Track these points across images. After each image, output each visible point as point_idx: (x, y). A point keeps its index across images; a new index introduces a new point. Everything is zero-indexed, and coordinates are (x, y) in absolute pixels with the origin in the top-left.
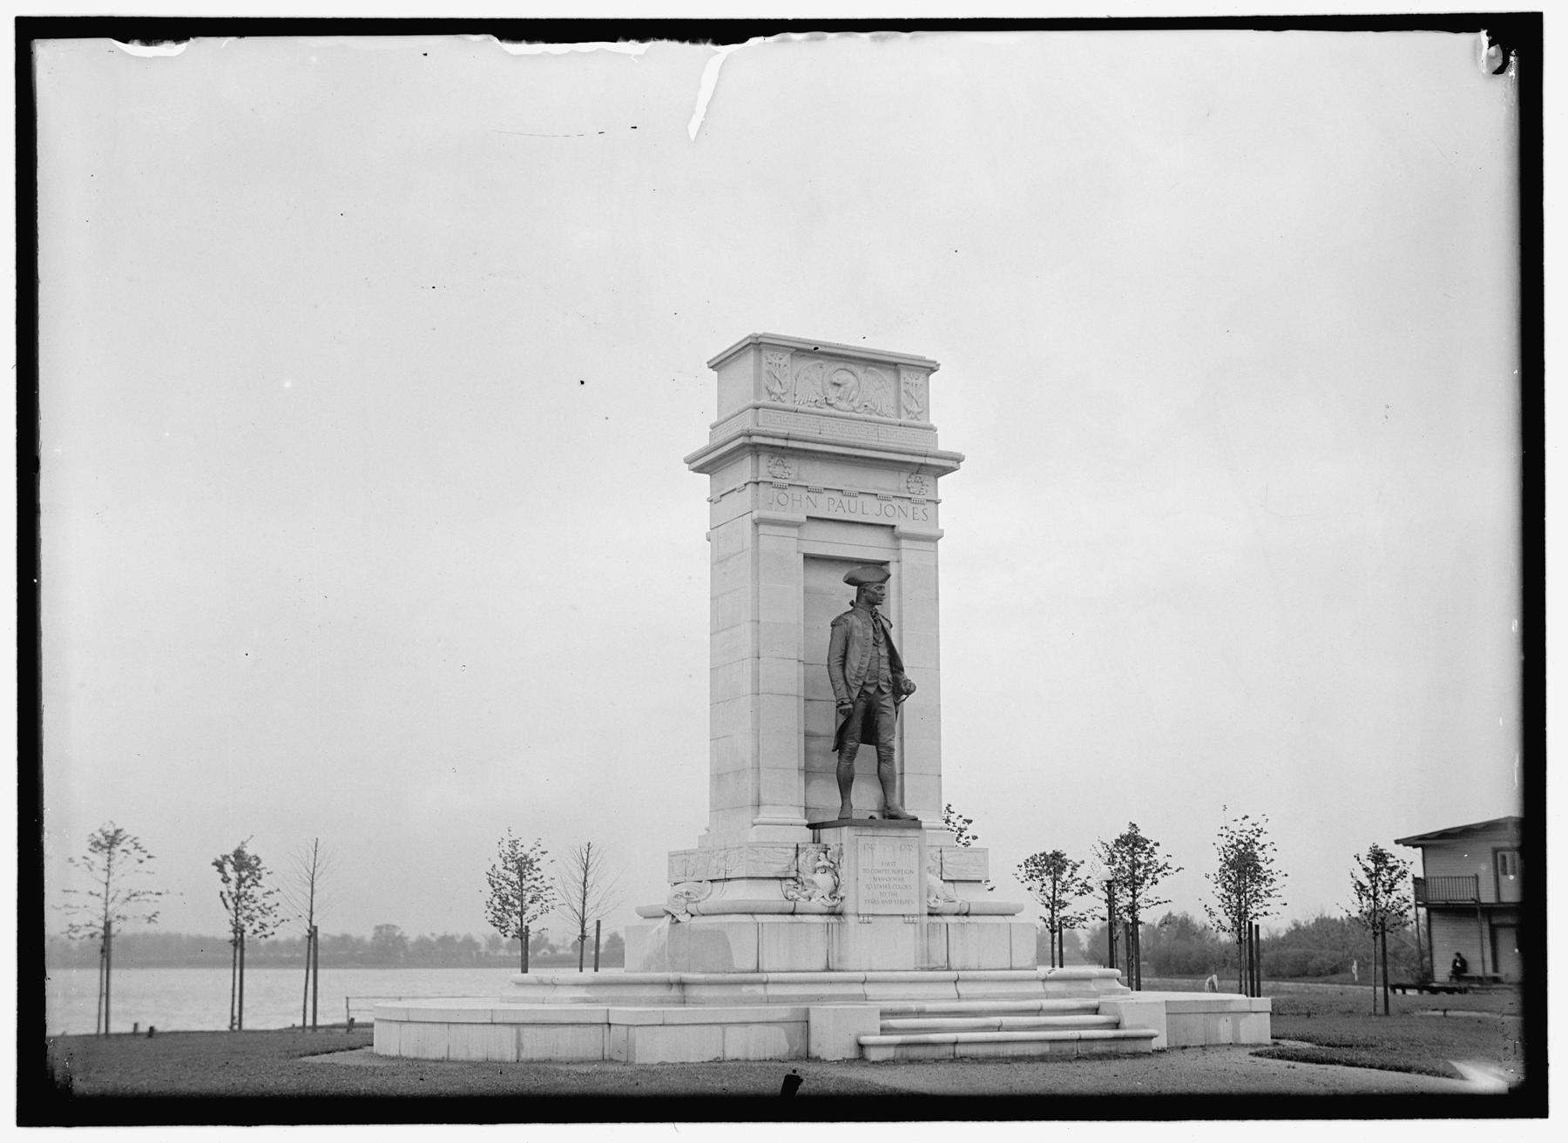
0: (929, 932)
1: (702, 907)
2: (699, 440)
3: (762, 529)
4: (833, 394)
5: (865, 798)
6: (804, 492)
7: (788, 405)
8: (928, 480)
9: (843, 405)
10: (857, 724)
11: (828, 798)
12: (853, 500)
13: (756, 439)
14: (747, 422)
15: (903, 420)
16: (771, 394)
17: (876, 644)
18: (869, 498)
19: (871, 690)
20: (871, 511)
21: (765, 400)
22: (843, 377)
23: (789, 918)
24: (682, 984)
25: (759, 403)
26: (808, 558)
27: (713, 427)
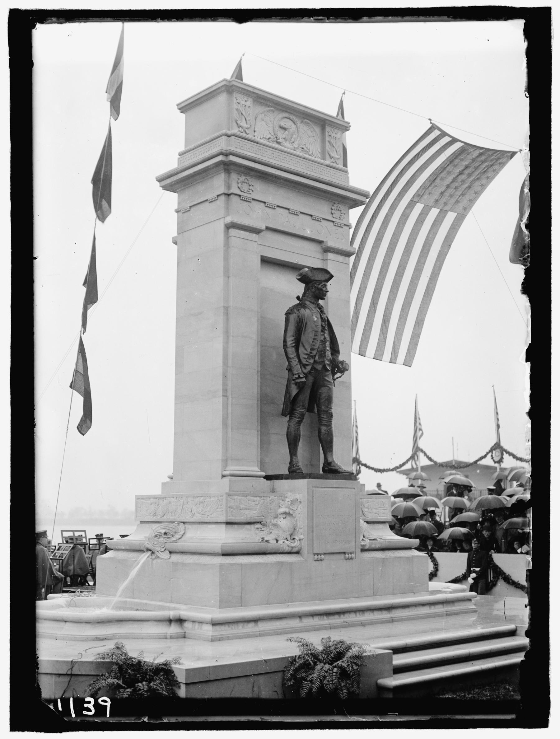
1: (180, 546)
2: (171, 164)
3: (233, 232)
4: (281, 135)
7: (250, 136)
8: (342, 207)
9: (287, 144)
10: (305, 396)
13: (232, 158)
14: (222, 145)
15: (328, 162)
16: (239, 126)
17: (323, 331)
18: (305, 217)
19: (319, 367)
21: (235, 131)
22: (287, 123)
24: (180, 621)
25: (229, 133)
26: (266, 261)
27: (180, 155)
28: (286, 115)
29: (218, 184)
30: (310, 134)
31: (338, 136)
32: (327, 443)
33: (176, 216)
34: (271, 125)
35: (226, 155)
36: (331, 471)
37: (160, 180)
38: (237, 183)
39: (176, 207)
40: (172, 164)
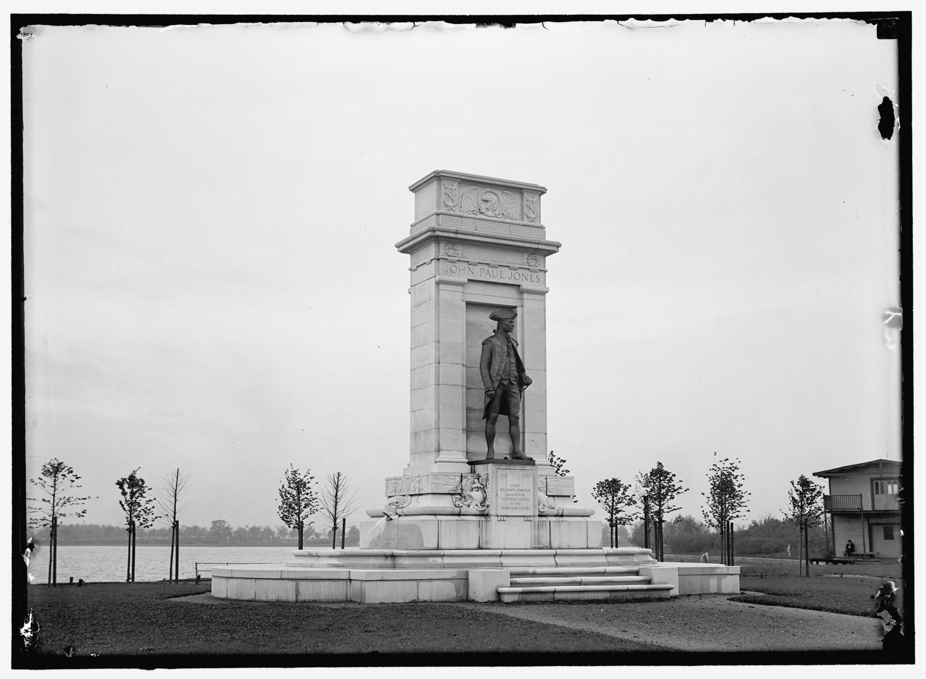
0: (539, 526)
1: (405, 511)
3: (441, 286)
4: (483, 206)
5: (502, 447)
6: (466, 265)
7: (457, 213)
9: (490, 213)
10: (497, 402)
11: (480, 447)
12: (495, 270)
13: (438, 233)
14: (432, 223)
15: (526, 222)
16: (447, 206)
17: (509, 355)
19: (506, 383)
20: (506, 276)
21: (443, 210)
22: (488, 196)
23: (457, 518)
24: (393, 556)
25: (440, 212)
26: (470, 304)
28: (489, 190)
29: (431, 251)
30: (509, 201)
31: (535, 199)
32: (514, 437)
33: (406, 278)
34: (475, 200)
35: (434, 230)
36: (518, 458)
37: (398, 246)
38: (444, 250)
39: (409, 266)
40: (406, 235)
